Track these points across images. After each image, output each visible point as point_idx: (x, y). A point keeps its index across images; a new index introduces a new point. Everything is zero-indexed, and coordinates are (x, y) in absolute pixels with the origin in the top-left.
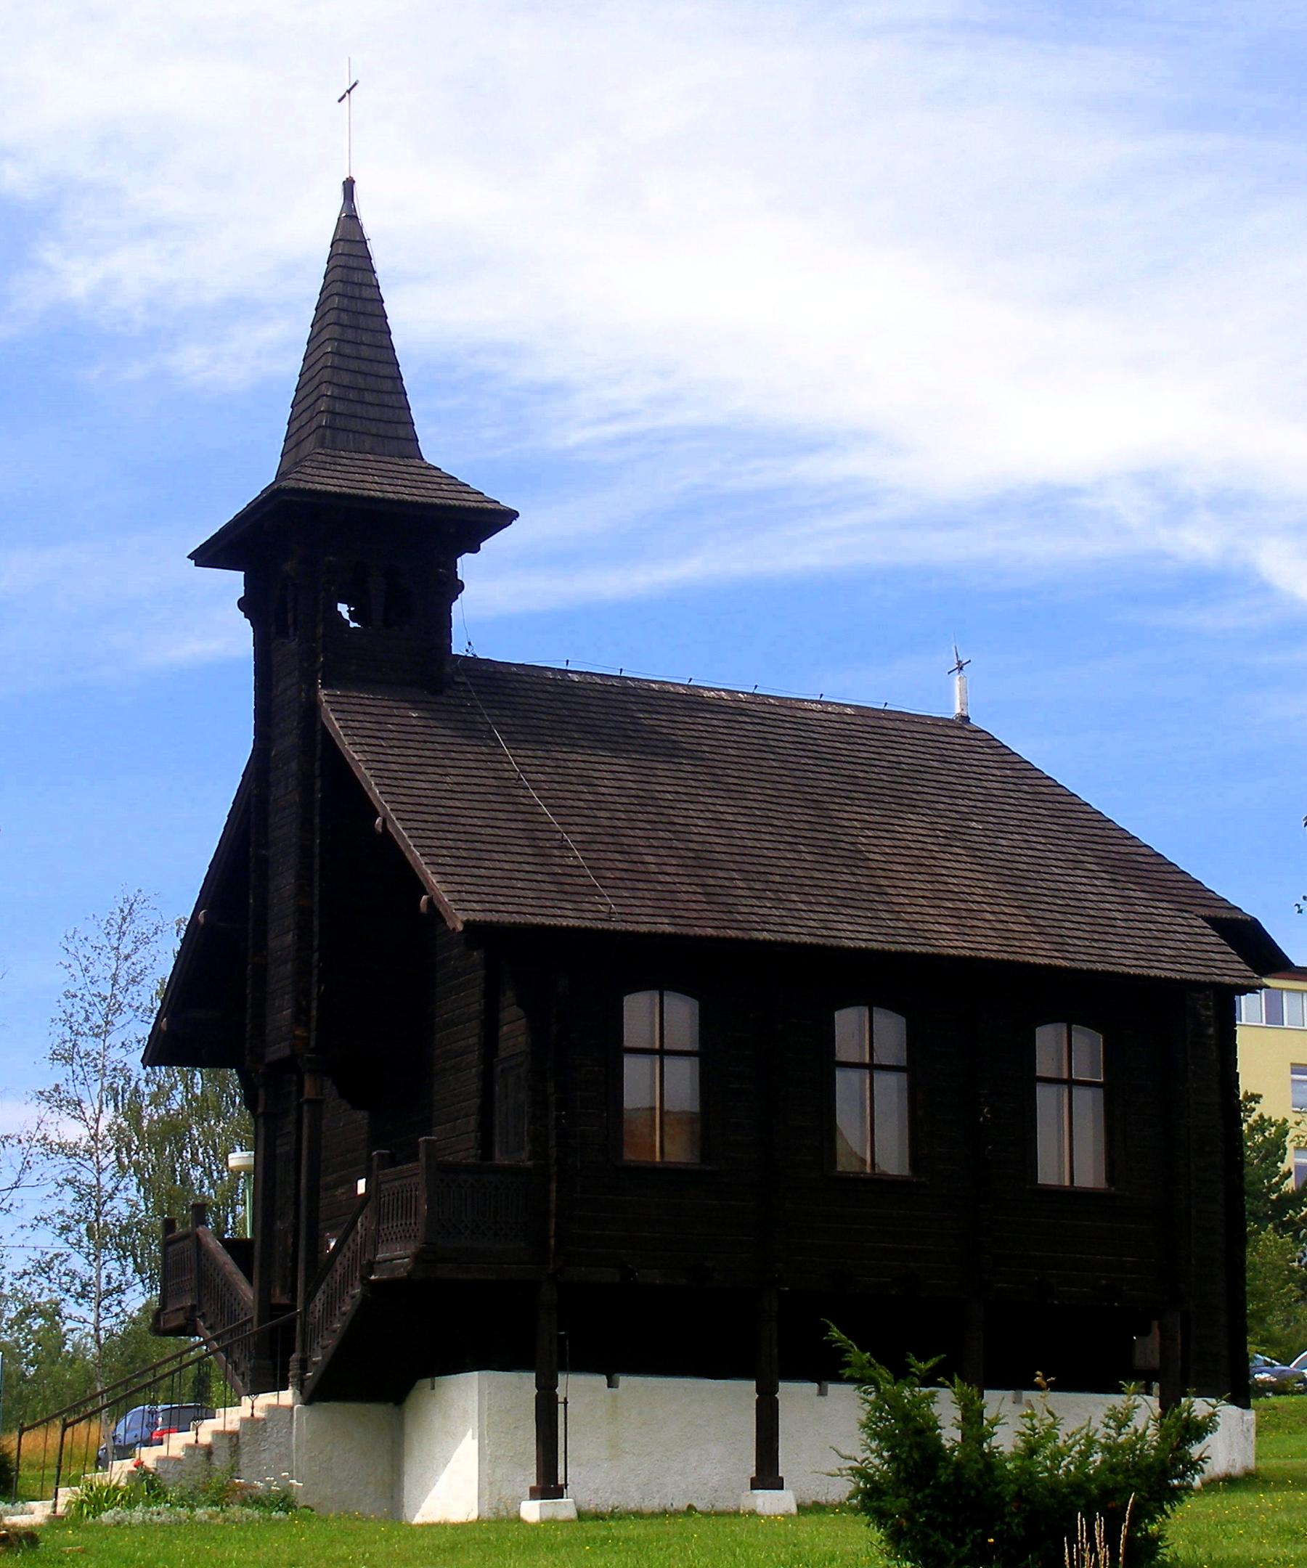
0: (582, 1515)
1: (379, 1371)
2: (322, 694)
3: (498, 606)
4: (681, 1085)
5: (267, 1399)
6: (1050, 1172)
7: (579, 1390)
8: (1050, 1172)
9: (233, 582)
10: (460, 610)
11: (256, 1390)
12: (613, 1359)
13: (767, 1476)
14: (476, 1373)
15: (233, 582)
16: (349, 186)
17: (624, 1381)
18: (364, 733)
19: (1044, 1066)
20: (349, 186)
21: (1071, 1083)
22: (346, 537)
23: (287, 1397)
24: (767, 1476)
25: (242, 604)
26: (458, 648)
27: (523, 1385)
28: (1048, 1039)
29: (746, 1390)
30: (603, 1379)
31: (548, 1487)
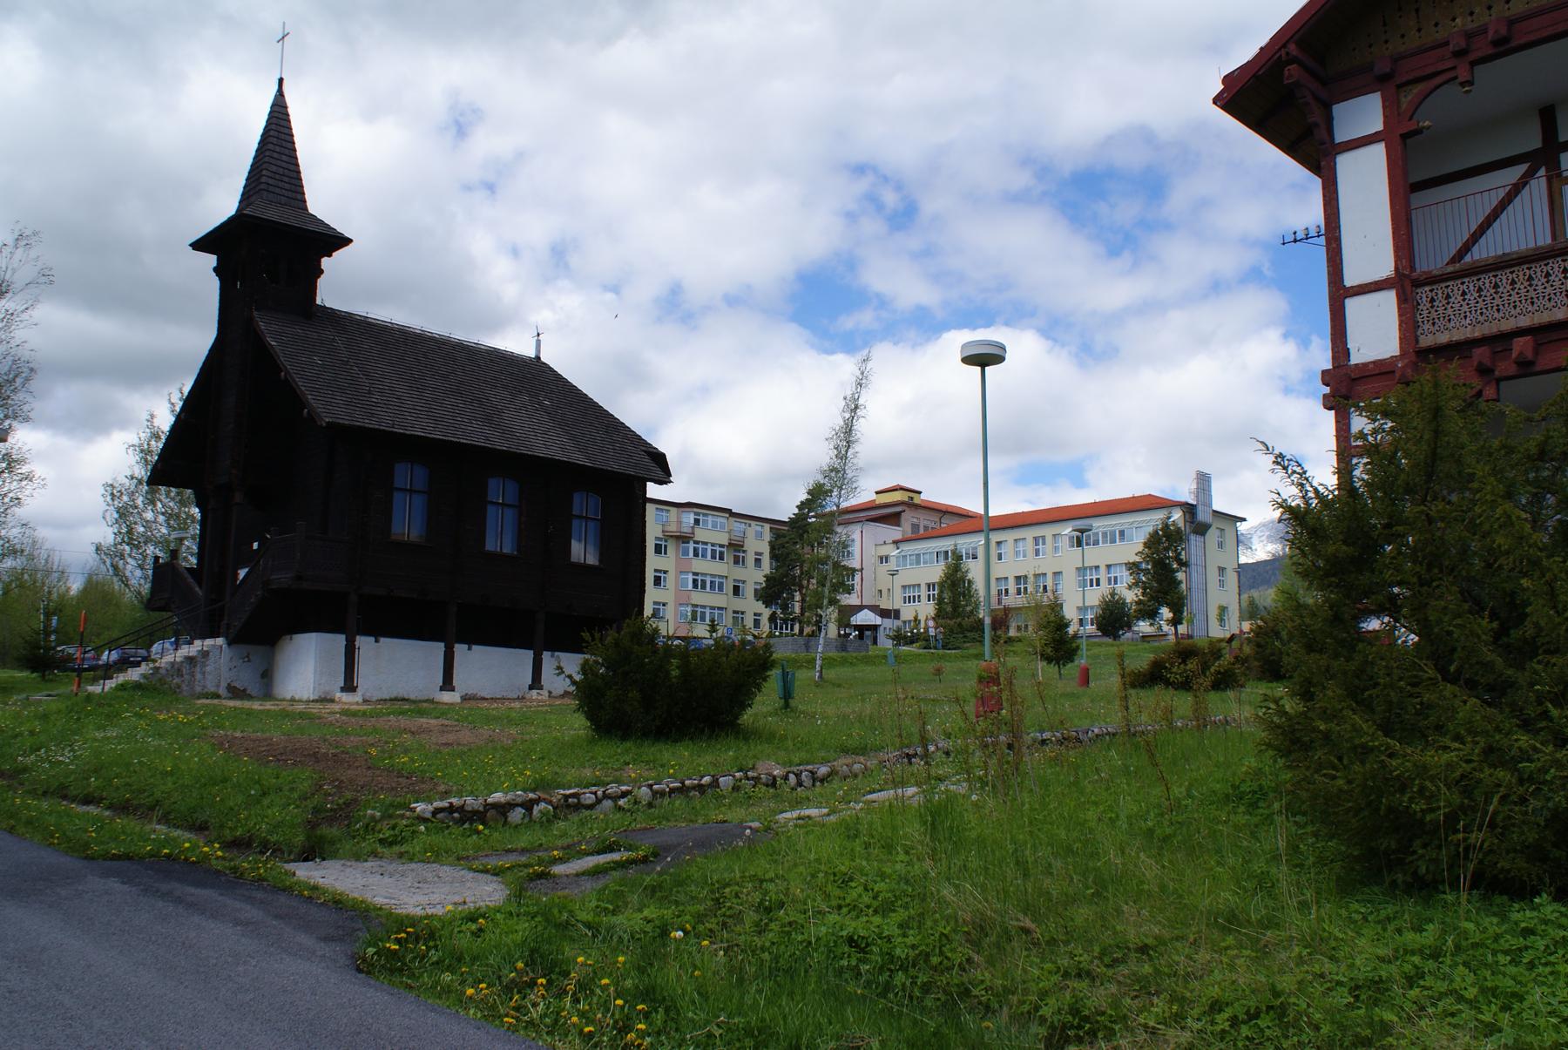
0: (365, 701)
1: (263, 630)
2: (255, 314)
3: (340, 285)
4: (1370, 628)
5: (209, 642)
6: (491, 545)
7: (364, 643)
8: (491, 545)
9: (211, 260)
10: (321, 282)
11: (203, 637)
12: (382, 627)
13: (447, 684)
14: (314, 635)
15: (211, 260)
16: (281, 81)
17: (385, 642)
18: (274, 332)
19: (398, 483)
20: (281, 81)
21: (587, 518)
22: (270, 243)
23: (220, 641)
24: (447, 684)
25: (215, 270)
26: (318, 302)
27: (340, 640)
28: (577, 499)
29: (530, 654)
30: (372, 639)
31: (349, 687)
